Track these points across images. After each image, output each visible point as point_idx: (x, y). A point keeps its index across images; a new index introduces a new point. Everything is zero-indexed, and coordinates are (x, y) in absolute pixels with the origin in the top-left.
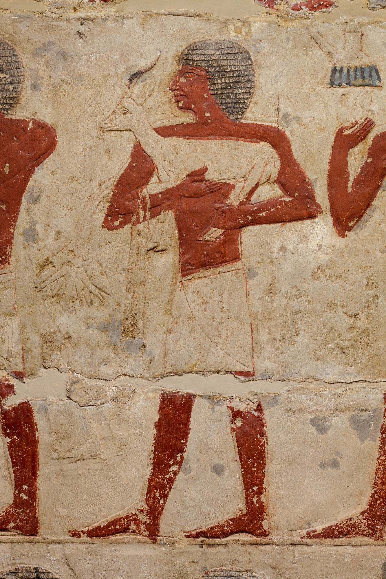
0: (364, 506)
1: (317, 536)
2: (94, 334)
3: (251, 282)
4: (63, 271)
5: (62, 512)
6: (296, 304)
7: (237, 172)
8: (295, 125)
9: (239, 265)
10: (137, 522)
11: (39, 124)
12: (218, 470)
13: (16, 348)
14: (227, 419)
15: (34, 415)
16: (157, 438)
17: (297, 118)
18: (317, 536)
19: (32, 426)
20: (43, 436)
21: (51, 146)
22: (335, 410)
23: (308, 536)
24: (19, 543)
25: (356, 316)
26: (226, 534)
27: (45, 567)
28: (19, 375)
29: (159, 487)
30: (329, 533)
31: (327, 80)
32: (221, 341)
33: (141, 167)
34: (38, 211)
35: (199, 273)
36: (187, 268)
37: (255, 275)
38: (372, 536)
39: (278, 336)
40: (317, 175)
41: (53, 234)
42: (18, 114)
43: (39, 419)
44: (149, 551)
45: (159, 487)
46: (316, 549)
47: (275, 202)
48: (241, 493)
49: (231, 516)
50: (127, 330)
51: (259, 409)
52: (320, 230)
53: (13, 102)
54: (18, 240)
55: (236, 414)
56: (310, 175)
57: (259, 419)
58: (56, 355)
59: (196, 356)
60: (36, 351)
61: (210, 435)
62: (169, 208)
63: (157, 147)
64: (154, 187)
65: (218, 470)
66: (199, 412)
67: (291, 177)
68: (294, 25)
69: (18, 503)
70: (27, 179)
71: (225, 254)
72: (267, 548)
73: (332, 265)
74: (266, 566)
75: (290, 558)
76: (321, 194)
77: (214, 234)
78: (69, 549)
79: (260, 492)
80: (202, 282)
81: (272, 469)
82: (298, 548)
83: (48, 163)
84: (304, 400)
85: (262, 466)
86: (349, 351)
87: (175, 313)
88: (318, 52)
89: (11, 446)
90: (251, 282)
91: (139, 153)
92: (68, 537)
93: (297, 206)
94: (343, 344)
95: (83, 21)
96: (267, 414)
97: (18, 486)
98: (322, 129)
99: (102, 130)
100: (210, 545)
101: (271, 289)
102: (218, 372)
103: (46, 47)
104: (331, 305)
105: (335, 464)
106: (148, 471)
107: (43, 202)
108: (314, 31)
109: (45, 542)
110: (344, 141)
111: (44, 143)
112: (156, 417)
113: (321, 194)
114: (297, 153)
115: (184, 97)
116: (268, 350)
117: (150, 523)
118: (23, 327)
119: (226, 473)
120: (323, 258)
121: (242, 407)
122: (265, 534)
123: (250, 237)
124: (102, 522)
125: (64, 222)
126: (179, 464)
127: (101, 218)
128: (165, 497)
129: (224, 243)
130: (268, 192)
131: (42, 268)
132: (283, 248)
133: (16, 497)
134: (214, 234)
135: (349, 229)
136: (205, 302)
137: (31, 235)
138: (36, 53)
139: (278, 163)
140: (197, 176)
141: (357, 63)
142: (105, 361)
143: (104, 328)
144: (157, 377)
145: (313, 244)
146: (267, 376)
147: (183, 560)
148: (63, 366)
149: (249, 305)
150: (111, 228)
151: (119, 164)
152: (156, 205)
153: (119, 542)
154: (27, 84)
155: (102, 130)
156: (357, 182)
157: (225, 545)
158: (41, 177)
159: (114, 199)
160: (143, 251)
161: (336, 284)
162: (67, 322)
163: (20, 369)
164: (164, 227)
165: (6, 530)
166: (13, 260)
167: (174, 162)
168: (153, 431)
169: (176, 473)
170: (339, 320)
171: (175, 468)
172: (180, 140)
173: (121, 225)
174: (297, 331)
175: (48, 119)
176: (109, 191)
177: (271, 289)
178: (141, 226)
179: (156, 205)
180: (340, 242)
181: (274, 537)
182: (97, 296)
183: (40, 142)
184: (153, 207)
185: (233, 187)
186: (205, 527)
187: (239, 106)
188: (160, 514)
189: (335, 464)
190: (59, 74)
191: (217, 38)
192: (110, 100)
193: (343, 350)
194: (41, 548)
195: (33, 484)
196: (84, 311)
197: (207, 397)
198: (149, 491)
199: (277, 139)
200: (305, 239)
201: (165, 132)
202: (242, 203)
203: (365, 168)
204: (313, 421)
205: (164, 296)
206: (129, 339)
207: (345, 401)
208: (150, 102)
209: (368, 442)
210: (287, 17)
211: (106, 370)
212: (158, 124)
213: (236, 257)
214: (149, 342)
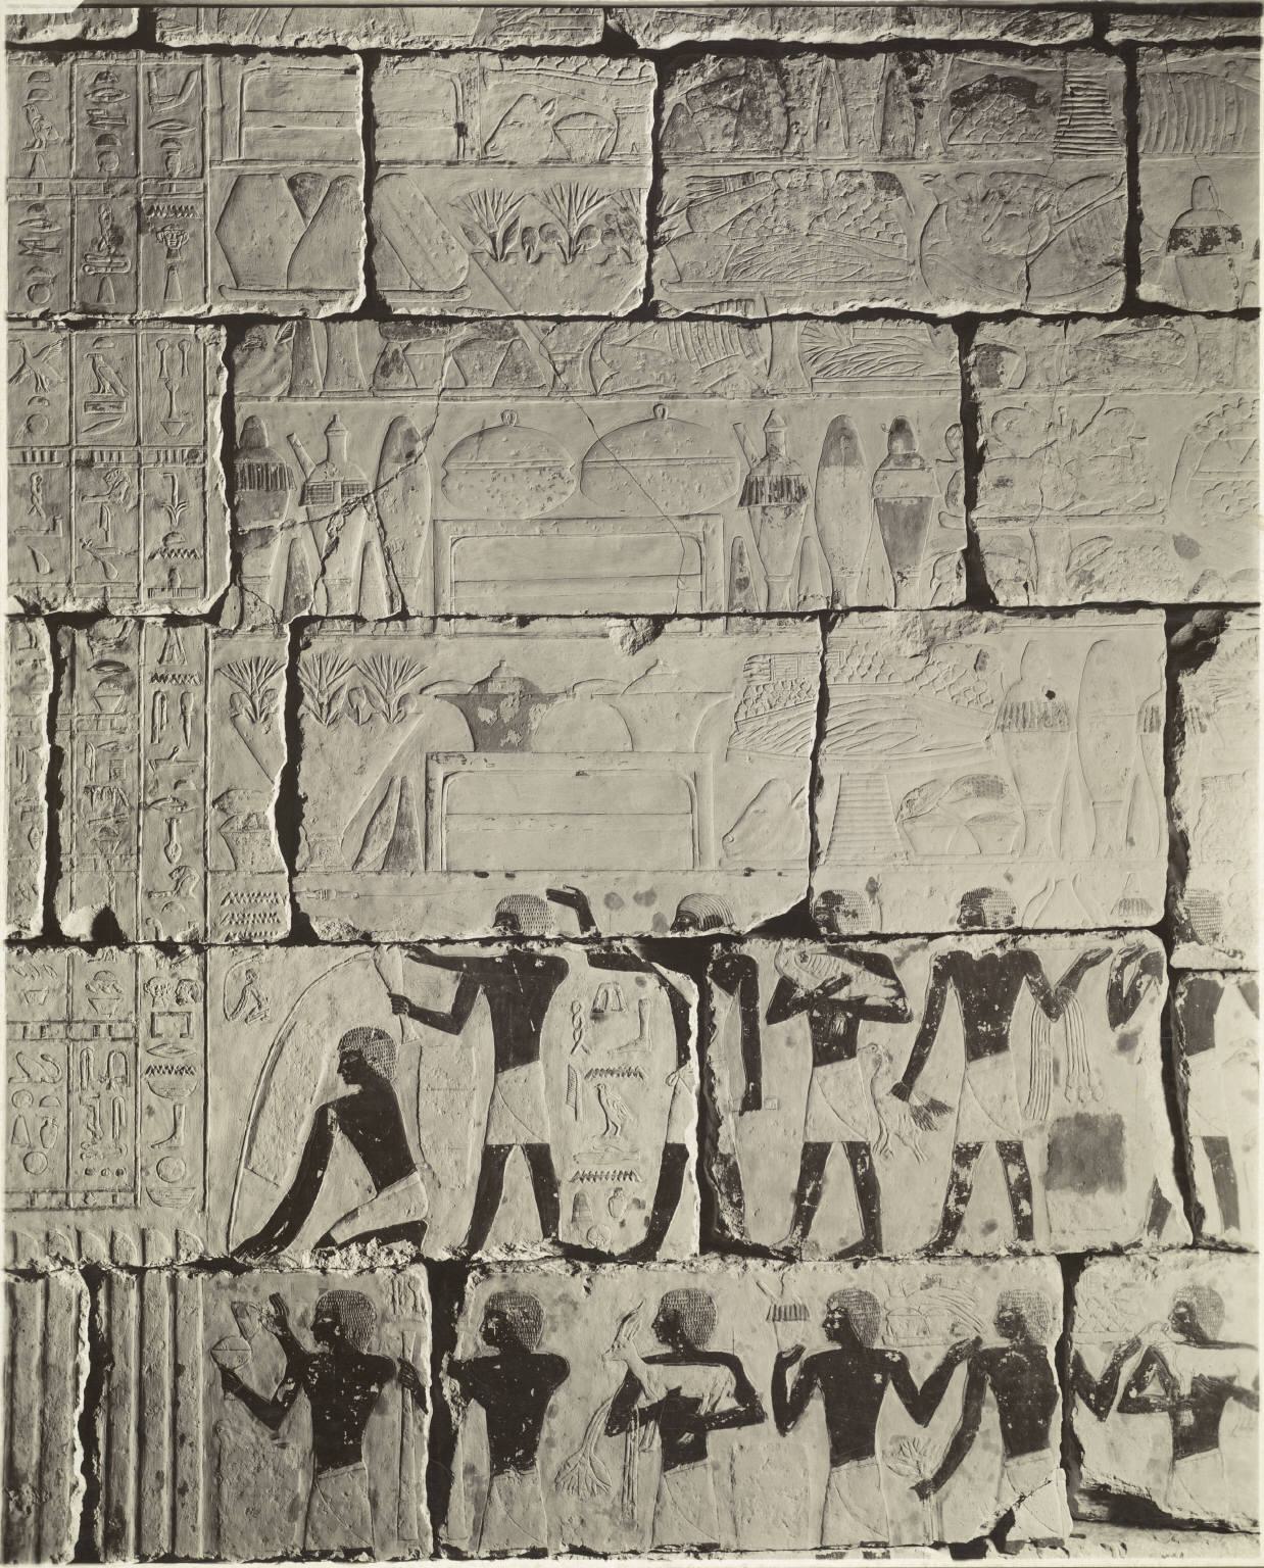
3: (617, 629)
40: (761, 1381)
47: (732, 1411)
63: (642, 1371)
64: (642, 1402)
67: (744, 1391)
76: (767, 1405)
77: (687, 1438)
80: (679, 1472)
93: (747, 1413)
110: (782, 1363)
130: (728, 1404)
134: (687, 1438)
140: (674, 1394)
150: (611, 1435)
158: (559, 1398)
167: (658, 1382)
173: (618, 1433)
183: (556, 1369)
187: (703, 1338)
201: (650, 1360)
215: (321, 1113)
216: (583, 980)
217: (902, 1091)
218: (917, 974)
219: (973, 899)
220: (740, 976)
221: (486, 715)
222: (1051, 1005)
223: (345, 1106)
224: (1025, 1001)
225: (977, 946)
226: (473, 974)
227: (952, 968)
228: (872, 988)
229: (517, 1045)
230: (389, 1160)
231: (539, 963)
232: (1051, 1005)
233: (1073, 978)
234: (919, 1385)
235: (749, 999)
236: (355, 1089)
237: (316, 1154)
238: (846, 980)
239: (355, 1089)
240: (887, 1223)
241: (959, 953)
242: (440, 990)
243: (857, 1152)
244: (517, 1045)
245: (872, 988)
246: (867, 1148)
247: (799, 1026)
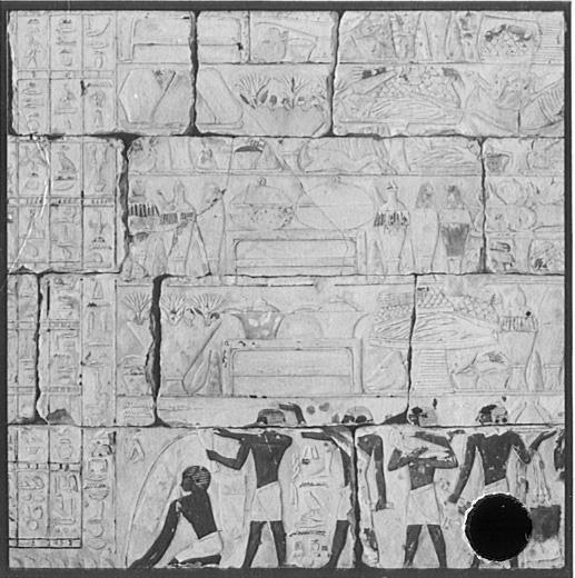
215: (173, 505)
216: (302, 447)
217: (454, 499)
218: (459, 445)
219: (487, 411)
220: (374, 446)
221: (253, 323)
222: (525, 459)
223: (183, 500)
224: (514, 457)
225: (489, 432)
226: (247, 442)
227: (475, 442)
228: (439, 452)
229: (267, 475)
230: (205, 526)
231: (278, 437)
232: (525, 459)
233: (536, 445)
234: (253, 566)
235: (379, 456)
236: (189, 493)
237: (172, 522)
238: (425, 450)
239: (189, 493)
240: (389, 497)
241: (479, 434)
242: (231, 449)
243: (435, 531)
244: (267, 475)
245: (439, 452)
246: (439, 527)
247: (404, 471)
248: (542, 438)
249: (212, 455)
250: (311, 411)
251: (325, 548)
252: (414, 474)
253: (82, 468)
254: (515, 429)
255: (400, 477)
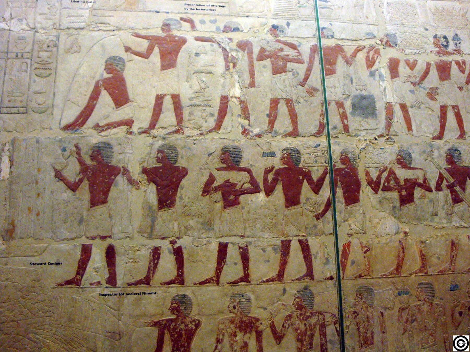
0: (277, 273)
1: (264, 282)
2: (199, 226)
3: (243, 211)
4: (190, 208)
5: (191, 277)
6: (256, 216)
7: (238, 180)
8: (254, 167)
9: (240, 206)
10: (213, 280)
11: (183, 168)
12: (236, 264)
13: (177, 230)
14: (238, 249)
15: (183, 249)
16: (218, 255)
17: (254, 165)
18: (264, 282)
19: (182, 252)
20: (185, 256)
21: (187, 173)
22: (268, 246)
23: (262, 282)
24: (179, 287)
25: (272, 219)
26: (238, 282)
27: (187, 294)
28: (178, 238)
29: (219, 269)
30: (268, 281)
31: (262, 155)
32: (235, 227)
33: (212, 179)
34: (183, 191)
35: (228, 208)
36: (225, 207)
37: (244, 208)
38: (280, 281)
39: (251, 225)
41: (187, 198)
42: (177, 165)
43: (184, 251)
44: (216, 288)
45: (219, 269)
46: (264, 285)
47: (249, 188)
48: (242, 270)
49: (240, 277)
50: (208, 225)
51: (247, 246)
52: (261, 196)
53: (176, 161)
54: (177, 199)
55: (240, 248)
56: (258, 181)
57: (247, 249)
58: (189, 232)
59: (228, 231)
60: (183, 231)
61: (233, 253)
62: (220, 190)
63: (216, 174)
64: (215, 184)
65: (236, 264)
66: (230, 247)
67: (253, 181)
68: (253, 141)
69: (178, 275)
70: (180, 183)
71: (235, 203)
72: (250, 286)
73: (265, 205)
74: (250, 291)
75: (257, 288)
76: (261, 186)
77: (232, 197)
78: (194, 288)
79: (248, 270)
80: (230, 211)
81: (251, 263)
82: (259, 286)
83: (186, 178)
84: (259, 243)
85: (248, 262)
86: (271, 229)
87: (222, 219)
88: (259, 148)
89: (176, 259)
90: (243, 211)
91: (211, 176)
92: (193, 285)
93: (255, 190)
94: (270, 227)
95: (195, 140)
96: (249, 247)
97: (178, 270)
98: (261, 168)
99: (201, 169)
100: (234, 286)
101: (249, 212)
102: (234, 236)
103: (185, 147)
104: (266, 216)
105: (268, 261)
106: (216, 265)
107: (184, 189)
108: (258, 143)
109: (186, 286)
110: (267, 171)
111: (185, 173)
112: (218, 249)
113: (261, 186)
114: (254, 175)
115: (224, 161)
116: (248, 229)
117: (216, 279)
118: (179, 224)
119: (238, 265)
120: (263, 203)
121: (242, 246)
122: (250, 282)
123: (242, 198)
124: (203, 280)
125: (190, 194)
126: (224, 262)
127: (201, 193)
128: (221, 272)
129: (235, 199)
130: (247, 186)
131: (184, 207)
132: (252, 201)
133: (178, 273)
134: (232, 197)
135: (269, 195)
136: (230, 216)
137: (181, 198)
138: (182, 148)
139: (249, 178)
140: (227, 181)
141: (270, 151)
142: (202, 234)
143: (202, 224)
144: (217, 238)
145: (260, 199)
146: (248, 237)
147: (226, 290)
148: (191, 235)
149: (243, 217)
151: (205, 179)
152: (216, 189)
153: (207, 286)
154: (180, 157)
155: (201, 169)
156: (271, 182)
157: (238, 286)
158: (184, 182)
159: (204, 188)
160: (213, 202)
161: (267, 210)
162: (192, 222)
163: (178, 236)
164: (218, 196)
165: (175, 283)
166: (176, 205)
167: (221, 177)
168: (217, 253)
169: (224, 265)
170: (268, 220)
171: (223, 264)
172: (222, 172)
173: (206, 195)
174: (256, 224)
175: (185, 166)
176: (203, 186)
177: (249, 212)
178: (212, 195)
179: (216, 189)
180: (267, 199)
181: (252, 283)
182: (200, 215)
183: (184, 172)
184: (215, 190)
185: (237, 184)
186: (233, 280)
187: (239, 162)
188: (219, 277)
189: (268, 261)
190: (189, 154)
191: (232, 144)
192: (203, 161)
193: (269, 228)
194: (186, 288)
195: (182, 269)
196: (196, 219)
197: (232, 243)
198: (216, 270)
199: (249, 171)
200: (257, 198)
201: (218, 169)
202: (240, 189)
203: (273, 179)
204: (262, 249)
205: (219, 215)
206: (209, 227)
207: (270, 243)
208: (214, 161)
209: (277, 254)
210: (250, 139)
211: (203, 236)
212: (216, 167)
213: (239, 204)
214: (215, 227)
215: (97, 82)
222: (348, 63)
230: (121, 99)
233: (354, 55)
237: (95, 96)
238: (281, 50)
247: (267, 62)
248: (358, 50)
249: (128, 49)
250: (202, 22)
251: (212, 115)
252: (225, 198)
253: (32, 55)
254: (340, 43)
255: (264, 67)
